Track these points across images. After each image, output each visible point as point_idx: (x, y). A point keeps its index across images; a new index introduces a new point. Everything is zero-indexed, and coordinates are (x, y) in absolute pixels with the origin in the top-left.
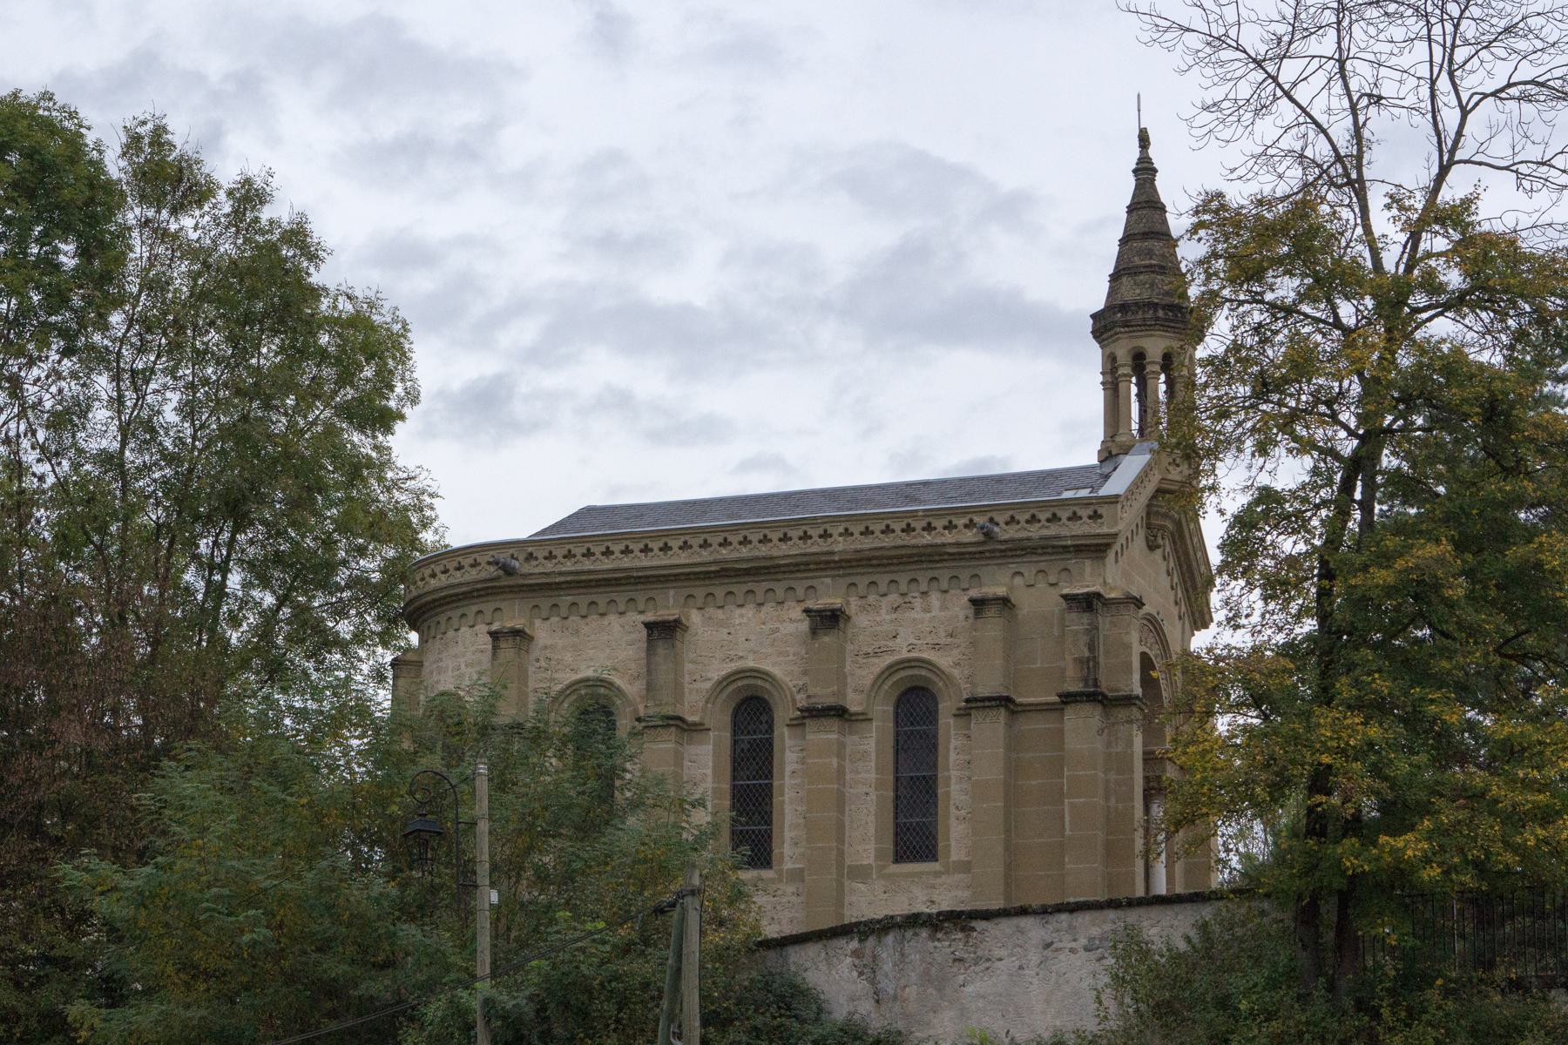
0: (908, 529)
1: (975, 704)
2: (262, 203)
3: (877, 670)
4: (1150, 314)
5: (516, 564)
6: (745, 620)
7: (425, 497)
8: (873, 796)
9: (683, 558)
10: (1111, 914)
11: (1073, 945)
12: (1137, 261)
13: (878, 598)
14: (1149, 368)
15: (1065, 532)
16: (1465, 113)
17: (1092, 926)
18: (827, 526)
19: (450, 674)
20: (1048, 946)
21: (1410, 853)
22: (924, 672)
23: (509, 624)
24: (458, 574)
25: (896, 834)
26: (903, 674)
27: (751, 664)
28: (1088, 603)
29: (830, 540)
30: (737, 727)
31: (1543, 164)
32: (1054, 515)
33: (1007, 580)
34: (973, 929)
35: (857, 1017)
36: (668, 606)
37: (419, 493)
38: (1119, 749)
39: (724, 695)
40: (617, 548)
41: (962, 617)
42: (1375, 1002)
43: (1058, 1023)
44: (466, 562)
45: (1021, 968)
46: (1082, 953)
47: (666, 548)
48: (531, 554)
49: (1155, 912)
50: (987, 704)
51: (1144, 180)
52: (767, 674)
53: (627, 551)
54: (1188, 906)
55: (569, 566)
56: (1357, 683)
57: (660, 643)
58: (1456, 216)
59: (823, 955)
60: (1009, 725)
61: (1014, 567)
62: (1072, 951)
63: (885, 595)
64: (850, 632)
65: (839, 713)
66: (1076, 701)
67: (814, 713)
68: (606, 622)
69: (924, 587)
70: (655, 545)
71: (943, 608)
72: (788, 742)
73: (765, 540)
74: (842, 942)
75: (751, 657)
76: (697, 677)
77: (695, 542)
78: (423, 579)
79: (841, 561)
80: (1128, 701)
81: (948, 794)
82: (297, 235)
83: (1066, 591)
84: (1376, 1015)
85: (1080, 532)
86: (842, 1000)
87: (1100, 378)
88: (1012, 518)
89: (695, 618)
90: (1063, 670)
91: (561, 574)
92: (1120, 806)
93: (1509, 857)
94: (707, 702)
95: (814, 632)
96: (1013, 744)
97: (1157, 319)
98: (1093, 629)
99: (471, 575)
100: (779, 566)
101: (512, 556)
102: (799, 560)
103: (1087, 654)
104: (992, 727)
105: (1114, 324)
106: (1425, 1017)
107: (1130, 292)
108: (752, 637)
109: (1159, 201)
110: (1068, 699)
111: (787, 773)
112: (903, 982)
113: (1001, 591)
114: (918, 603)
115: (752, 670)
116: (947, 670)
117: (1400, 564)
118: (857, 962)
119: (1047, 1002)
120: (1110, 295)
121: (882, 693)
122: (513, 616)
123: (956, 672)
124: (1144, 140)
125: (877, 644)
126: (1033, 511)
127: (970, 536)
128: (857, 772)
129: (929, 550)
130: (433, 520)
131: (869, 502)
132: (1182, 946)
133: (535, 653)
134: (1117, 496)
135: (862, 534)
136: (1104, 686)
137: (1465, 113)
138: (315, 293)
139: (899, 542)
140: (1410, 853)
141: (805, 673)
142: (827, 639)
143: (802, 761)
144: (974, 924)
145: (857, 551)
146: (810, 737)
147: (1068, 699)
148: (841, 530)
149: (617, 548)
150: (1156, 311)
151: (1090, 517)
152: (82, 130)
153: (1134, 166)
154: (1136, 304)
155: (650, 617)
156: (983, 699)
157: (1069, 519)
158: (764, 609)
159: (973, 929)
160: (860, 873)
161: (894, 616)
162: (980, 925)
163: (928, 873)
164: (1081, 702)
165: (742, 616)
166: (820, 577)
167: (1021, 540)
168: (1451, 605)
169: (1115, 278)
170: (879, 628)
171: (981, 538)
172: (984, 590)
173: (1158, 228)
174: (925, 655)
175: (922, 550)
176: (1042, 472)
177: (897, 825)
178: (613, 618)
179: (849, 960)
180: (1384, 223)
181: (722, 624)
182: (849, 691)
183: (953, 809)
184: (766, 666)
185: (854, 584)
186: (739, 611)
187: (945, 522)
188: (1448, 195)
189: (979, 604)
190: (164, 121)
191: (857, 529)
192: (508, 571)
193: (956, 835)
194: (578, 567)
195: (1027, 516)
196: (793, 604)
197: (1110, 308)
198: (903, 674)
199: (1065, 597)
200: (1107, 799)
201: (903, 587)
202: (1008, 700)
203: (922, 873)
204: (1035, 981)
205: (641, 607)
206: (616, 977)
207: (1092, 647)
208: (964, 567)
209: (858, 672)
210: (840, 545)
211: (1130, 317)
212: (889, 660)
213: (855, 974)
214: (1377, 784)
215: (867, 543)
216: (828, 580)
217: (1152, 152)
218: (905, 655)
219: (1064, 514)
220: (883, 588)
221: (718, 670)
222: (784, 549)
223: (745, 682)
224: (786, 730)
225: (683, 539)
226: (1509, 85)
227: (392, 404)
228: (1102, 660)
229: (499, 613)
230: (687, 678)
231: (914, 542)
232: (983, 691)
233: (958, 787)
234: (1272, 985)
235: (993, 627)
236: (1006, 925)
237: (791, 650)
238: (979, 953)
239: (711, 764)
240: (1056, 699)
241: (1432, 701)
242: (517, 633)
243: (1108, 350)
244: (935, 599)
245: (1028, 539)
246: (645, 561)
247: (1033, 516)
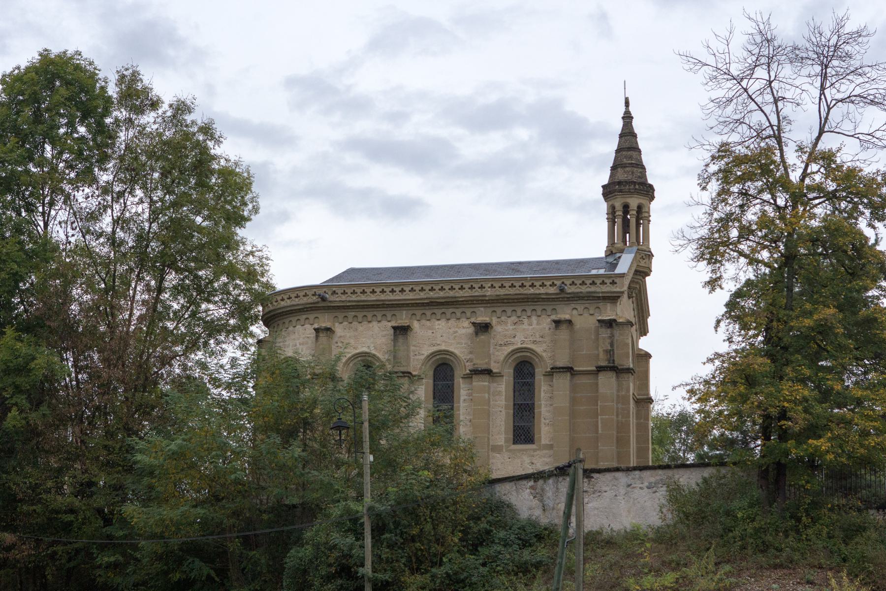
0: (522, 286)
1: (555, 370)
2: (190, 112)
3: (506, 353)
4: (632, 187)
5: (327, 296)
6: (441, 327)
7: (264, 260)
8: (504, 413)
9: (411, 296)
10: (660, 472)
11: (641, 486)
12: (625, 161)
15: (598, 290)
16: (829, 109)
17: (649, 477)
18: (483, 283)
19: (291, 348)
20: (629, 486)
21: (823, 448)
22: (528, 354)
23: (324, 325)
24: (297, 300)
25: (514, 431)
26: (519, 355)
27: (443, 347)
28: (610, 324)
30: (436, 378)
31: (869, 135)
32: (593, 282)
33: (569, 311)
34: (592, 477)
35: (534, 518)
36: (403, 319)
37: (261, 258)
38: (623, 393)
39: (430, 362)
40: (378, 290)
41: (547, 329)
42: (799, 515)
43: (634, 521)
44: (301, 294)
45: (616, 496)
46: (646, 489)
47: (402, 291)
48: (334, 291)
49: (681, 471)
51: (628, 122)
52: (452, 353)
53: (383, 292)
54: (698, 469)
55: (354, 298)
56: (794, 370)
57: (400, 336)
58: (828, 158)
59: (514, 488)
60: (571, 380)
61: (573, 306)
62: (641, 488)
63: (510, 317)
64: (493, 333)
65: (488, 372)
67: (477, 372)
68: (371, 325)
69: (529, 313)
70: (397, 289)
71: (538, 324)
72: (462, 386)
73: (452, 289)
74: (525, 482)
75: (443, 344)
76: (417, 353)
77: (417, 288)
78: (276, 301)
79: (489, 300)
80: (629, 371)
81: (540, 412)
82: (207, 130)
83: (600, 318)
84: (799, 520)
85: (606, 290)
86: (525, 509)
87: (606, 216)
88: (573, 282)
89: (416, 325)
90: (598, 355)
91: (349, 301)
92: (624, 420)
93: (862, 451)
94: (422, 365)
95: (477, 333)
96: (574, 389)
97: (636, 189)
98: (612, 337)
99: (305, 300)
100: (458, 301)
101: (325, 292)
102: (468, 299)
103: (609, 348)
104: (563, 382)
105: (615, 191)
106: (821, 522)
107: (621, 176)
109: (634, 133)
110: (600, 369)
111: (461, 401)
112: (558, 501)
113: (567, 317)
114: (526, 321)
115: (444, 351)
116: (540, 353)
117: (815, 317)
118: (533, 491)
119: (629, 511)
120: (611, 177)
121: (508, 363)
122: (325, 321)
123: (544, 354)
124: (627, 103)
125: (506, 340)
126: (583, 279)
127: (552, 290)
129: (532, 296)
130: (268, 271)
132: (694, 486)
133: (336, 339)
134: (624, 274)
135: (500, 287)
136: (619, 362)
137: (829, 109)
138: (214, 158)
139: (518, 292)
140: (823, 448)
141: (471, 353)
142: (483, 337)
143: (470, 395)
144: (593, 475)
145: (497, 296)
146: (474, 384)
147: (600, 369)
148: (489, 285)
149: (378, 290)
150: (635, 185)
151: (611, 283)
152: (97, 72)
153: (622, 115)
154: (626, 182)
155: (394, 324)
156: (560, 368)
157: (600, 284)
158: (450, 321)
159: (592, 477)
160: (497, 449)
161: (514, 327)
162: (595, 475)
163: (531, 449)
165: (439, 325)
167: (578, 293)
168: (836, 335)
169: (614, 168)
170: (507, 333)
171: (558, 291)
172: (559, 316)
173: (634, 145)
174: (529, 346)
175: (529, 296)
176: (577, 260)
177: (514, 426)
178: (375, 323)
179: (528, 490)
180: (792, 157)
181: (430, 328)
182: (492, 362)
183: (542, 419)
184: (451, 349)
185: (494, 311)
186: (437, 322)
187: (540, 283)
188: (822, 146)
189: (557, 323)
190: (138, 69)
191: (497, 285)
192: (323, 299)
193: (544, 431)
194: (359, 299)
195: (590, 281)
196: (464, 320)
198: (519, 355)
199: (599, 321)
200: (617, 416)
201: (519, 313)
202: (572, 368)
204: (623, 502)
205: (389, 319)
206: (428, 497)
207: (612, 344)
209: (497, 353)
210: (489, 292)
211: (622, 187)
212: (511, 348)
213: (532, 497)
214: (807, 416)
215: (502, 292)
216: (482, 309)
217: (631, 109)
218: (519, 346)
219: (598, 282)
220: (509, 313)
221: (427, 351)
222: (461, 293)
223: (441, 356)
224: (461, 380)
225: (411, 286)
226: (849, 97)
227: (246, 213)
228: (615, 351)
229: (317, 319)
230: (412, 354)
231: (526, 292)
232: (560, 364)
233: (545, 409)
234: (751, 506)
235: (564, 334)
236: (608, 476)
237: (463, 342)
238: (595, 488)
240: (594, 368)
241: (828, 379)
242: (328, 329)
243: (611, 203)
244: (534, 319)
245: (581, 293)
246: (392, 297)
247: (583, 282)
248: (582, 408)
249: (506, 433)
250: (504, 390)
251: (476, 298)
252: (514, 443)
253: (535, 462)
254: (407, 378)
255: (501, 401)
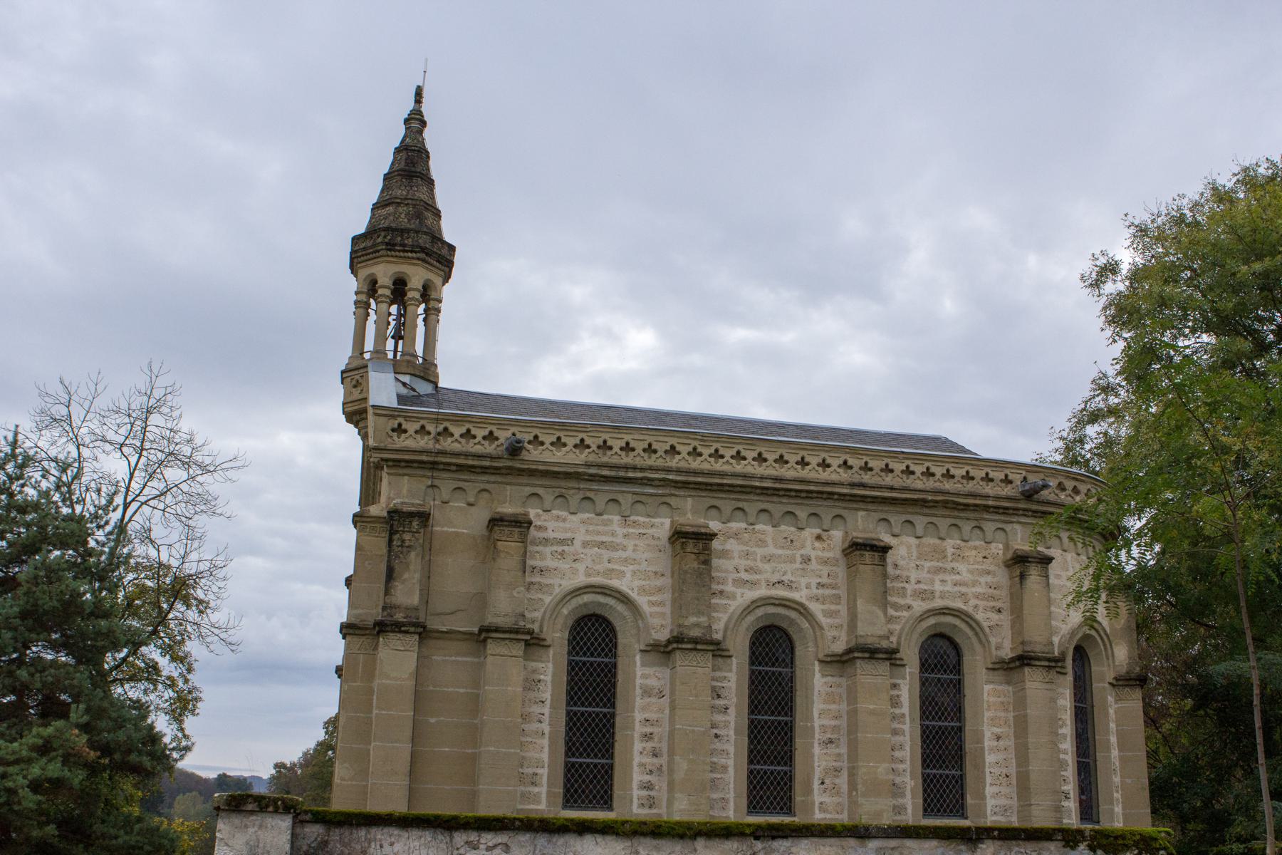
14: (410, 294)
29: (632, 454)
87: (443, 306)
111: (816, 714)
131: (473, 406)
166: (1012, 522)
197: (371, 232)
201: (827, 520)
208: (943, 516)
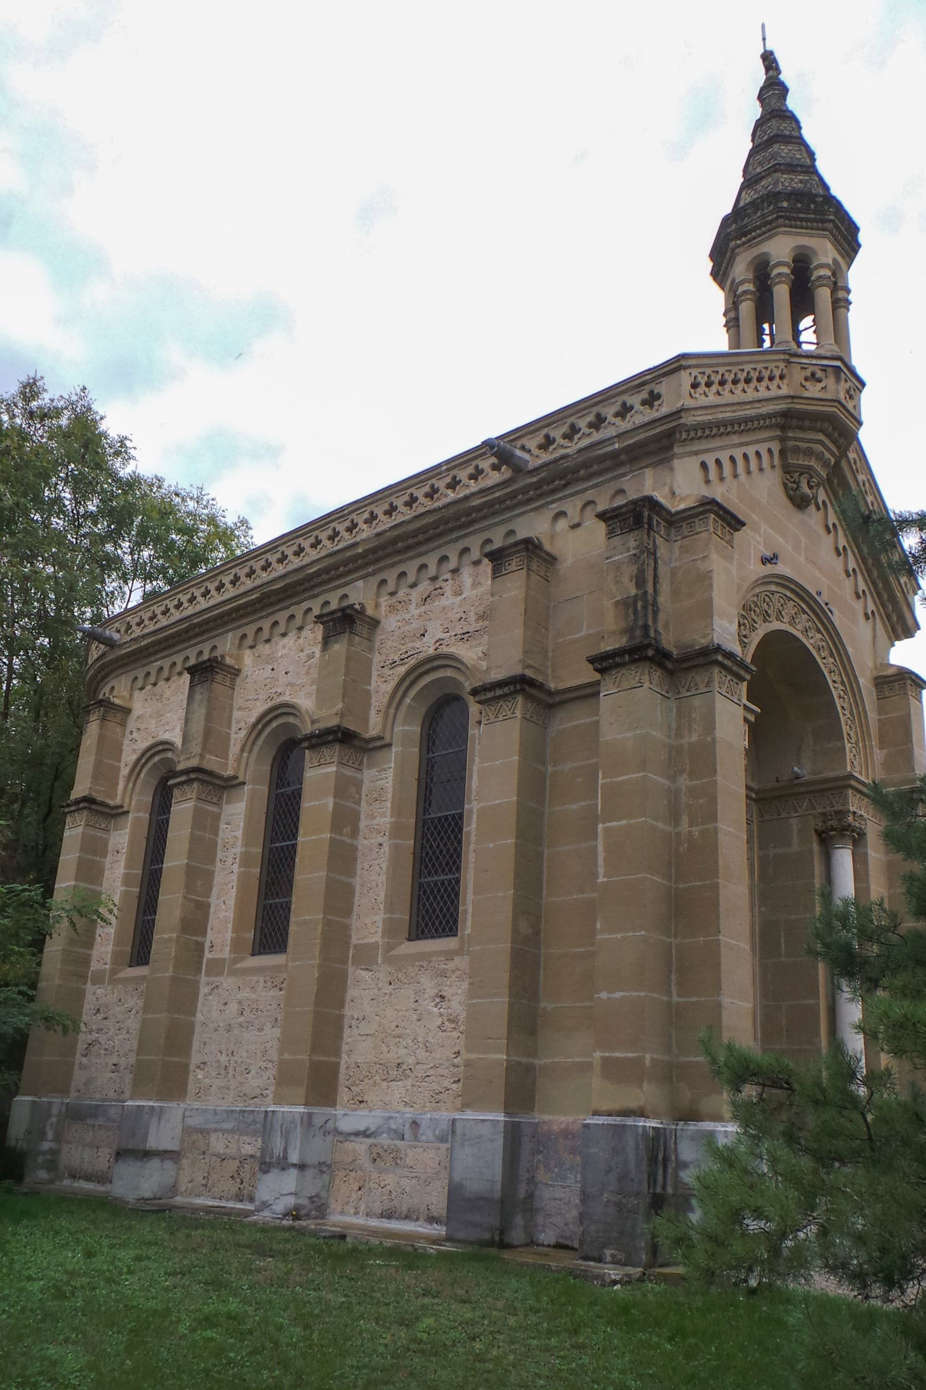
8: (386, 848)
13: (408, 590)
38: (694, 738)
39: (260, 742)
50: (499, 692)
66: (617, 666)
87: (851, 297)
102: (326, 563)
103: (633, 591)
108: (291, 669)
114: (448, 588)
121: (403, 708)
126: (570, 421)
128: (374, 818)
129: (452, 510)
158: (304, 633)
163: (438, 953)
164: (623, 665)
165: (284, 647)
170: (407, 628)
203: (430, 954)
216: (360, 583)
228: (663, 599)
239: (242, 824)
248: (574, 807)
249: (390, 907)
250: (390, 785)
251: (339, 557)
252: (410, 939)
253: (447, 992)
254: (85, 812)
255: (383, 815)
